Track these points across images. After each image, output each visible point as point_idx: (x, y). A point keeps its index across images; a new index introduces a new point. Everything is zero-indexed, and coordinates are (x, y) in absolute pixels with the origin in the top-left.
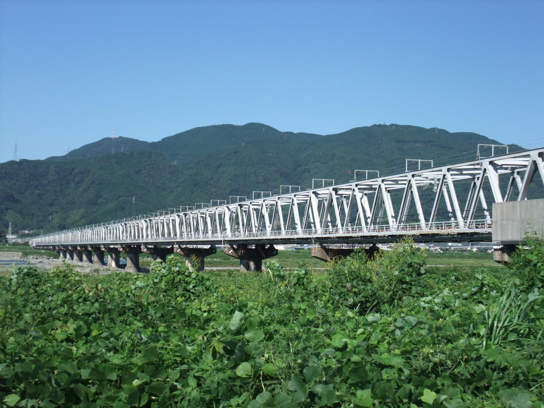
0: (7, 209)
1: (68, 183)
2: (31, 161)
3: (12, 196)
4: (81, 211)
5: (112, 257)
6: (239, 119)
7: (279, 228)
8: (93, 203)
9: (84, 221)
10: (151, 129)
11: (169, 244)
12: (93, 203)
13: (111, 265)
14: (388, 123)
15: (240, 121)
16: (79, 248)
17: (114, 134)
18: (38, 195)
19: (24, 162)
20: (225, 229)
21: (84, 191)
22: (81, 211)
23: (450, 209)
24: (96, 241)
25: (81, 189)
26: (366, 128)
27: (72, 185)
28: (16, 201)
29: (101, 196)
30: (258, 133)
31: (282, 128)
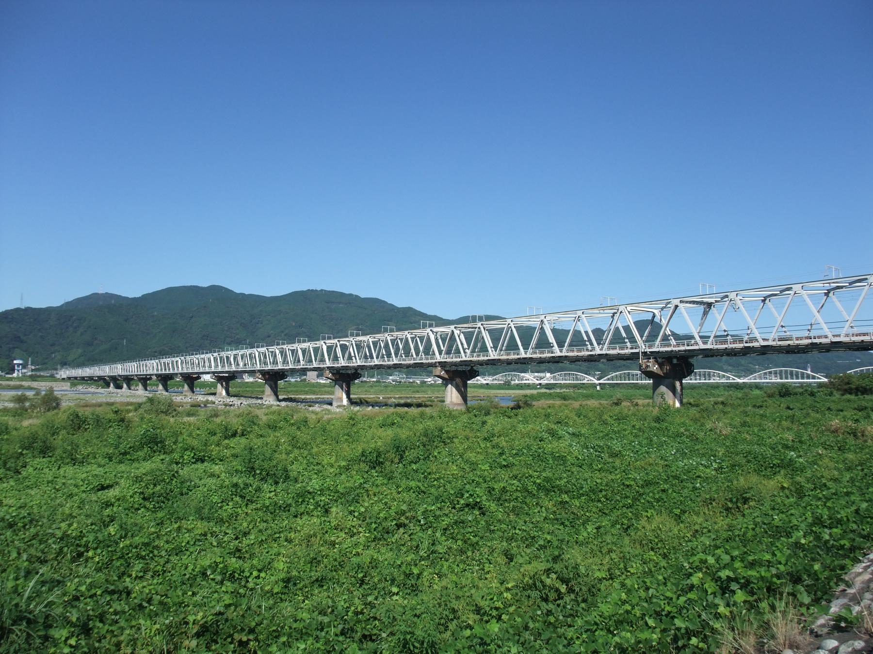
0: (14, 348)
1: (67, 328)
2: (35, 309)
3: (19, 337)
4: (80, 351)
5: (222, 385)
6: (204, 282)
7: (299, 361)
8: (90, 344)
9: (82, 358)
10: (132, 286)
11: (196, 373)
12: (90, 344)
13: (221, 394)
14: (319, 289)
15: (204, 284)
16: (675, 361)
17: (101, 291)
18: (41, 337)
19: (28, 309)
20: (231, 364)
21: (82, 334)
22: (80, 351)
23: (586, 338)
24: (101, 374)
25: (79, 333)
26: (303, 291)
27: (71, 329)
28: (22, 342)
29: (96, 339)
30: (218, 295)
31: (237, 290)
